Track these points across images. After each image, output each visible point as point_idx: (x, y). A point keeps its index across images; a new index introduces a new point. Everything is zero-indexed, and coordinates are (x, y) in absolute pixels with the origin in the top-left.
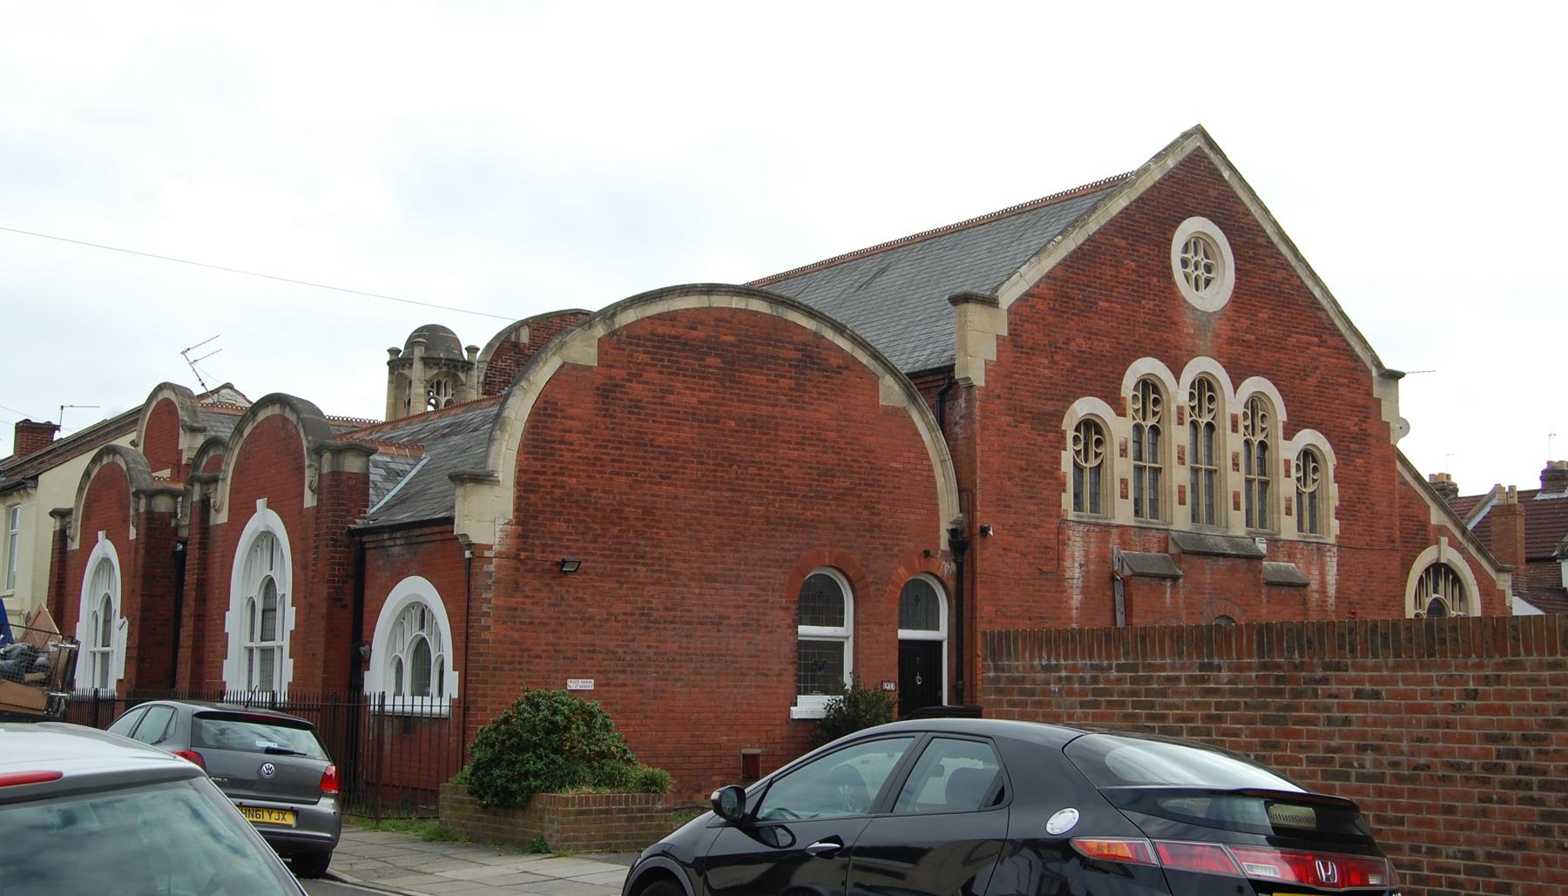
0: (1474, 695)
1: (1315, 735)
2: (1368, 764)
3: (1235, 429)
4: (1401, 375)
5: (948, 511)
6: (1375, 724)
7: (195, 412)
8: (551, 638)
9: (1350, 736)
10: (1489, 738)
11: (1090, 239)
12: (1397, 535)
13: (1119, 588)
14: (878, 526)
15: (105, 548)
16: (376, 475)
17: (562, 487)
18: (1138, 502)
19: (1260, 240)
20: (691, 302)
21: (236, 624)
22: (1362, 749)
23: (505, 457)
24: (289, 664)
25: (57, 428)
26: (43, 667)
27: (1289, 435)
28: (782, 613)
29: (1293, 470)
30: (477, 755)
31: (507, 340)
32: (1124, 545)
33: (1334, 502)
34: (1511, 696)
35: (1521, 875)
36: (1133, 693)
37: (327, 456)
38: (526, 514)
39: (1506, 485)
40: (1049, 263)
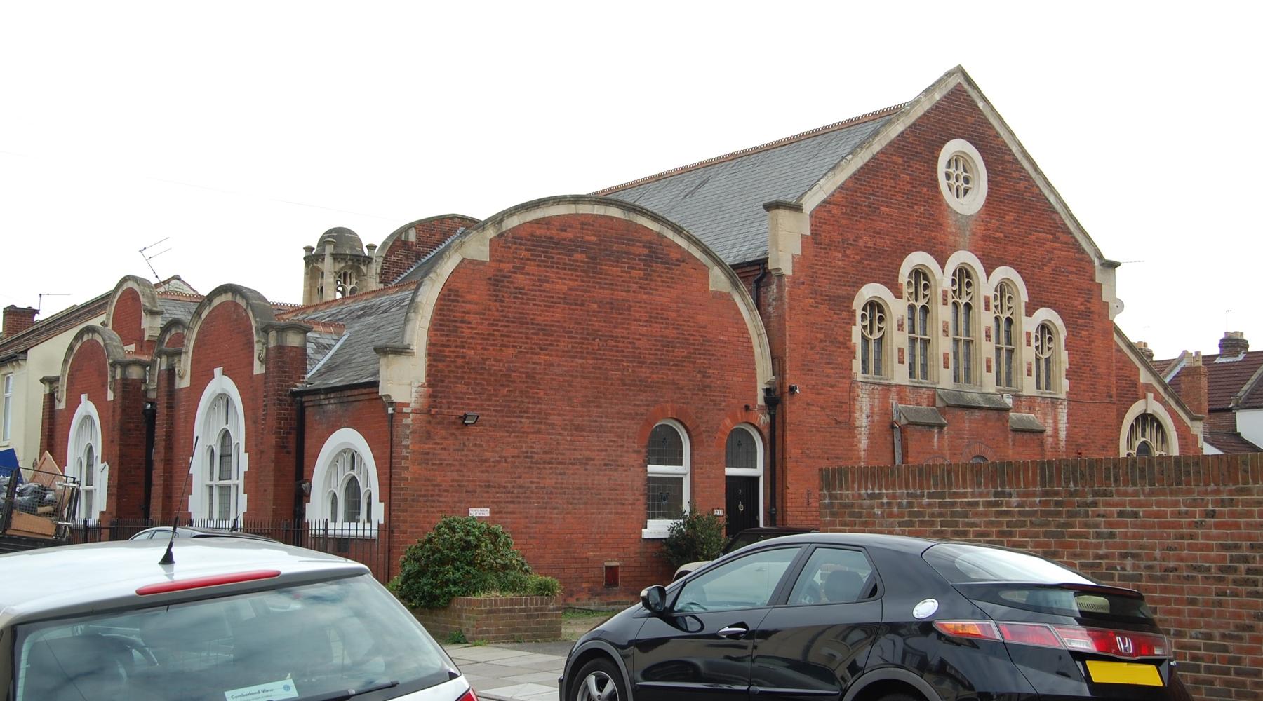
0: (1212, 514)
1: (1086, 546)
2: (1128, 568)
3: (987, 308)
4: (1118, 265)
5: (764, 374)
6: (1135, 536)
7: (153, 298)
8: (456, 476)
9: (1114, 546)
10: (1224, 547)
11: (874, 158)
12: (1114, 392)
13: (897, 435)
15: (87, 407)
16: (310, 348)
17: (463, 357)
18: (912, 366)
19: (1007, 157)
20: (562, 210)
21: (199, 468)
22: (1124, 556)
23: (418, 334)
24: (243, 498)
25: (37, 312)
26: (51, 502)
27: (1030, 313)
28: (635, 455)
29: (1033, 340)
30: (407, 568)
31: (398, 239)
32: (901, 400)
33: (1065, 365)
34: (1241, 515)
35: (1250, 651)
36: (941, 515)
37: (273, 334)
39: (1192, 351)
40: (841, 177)
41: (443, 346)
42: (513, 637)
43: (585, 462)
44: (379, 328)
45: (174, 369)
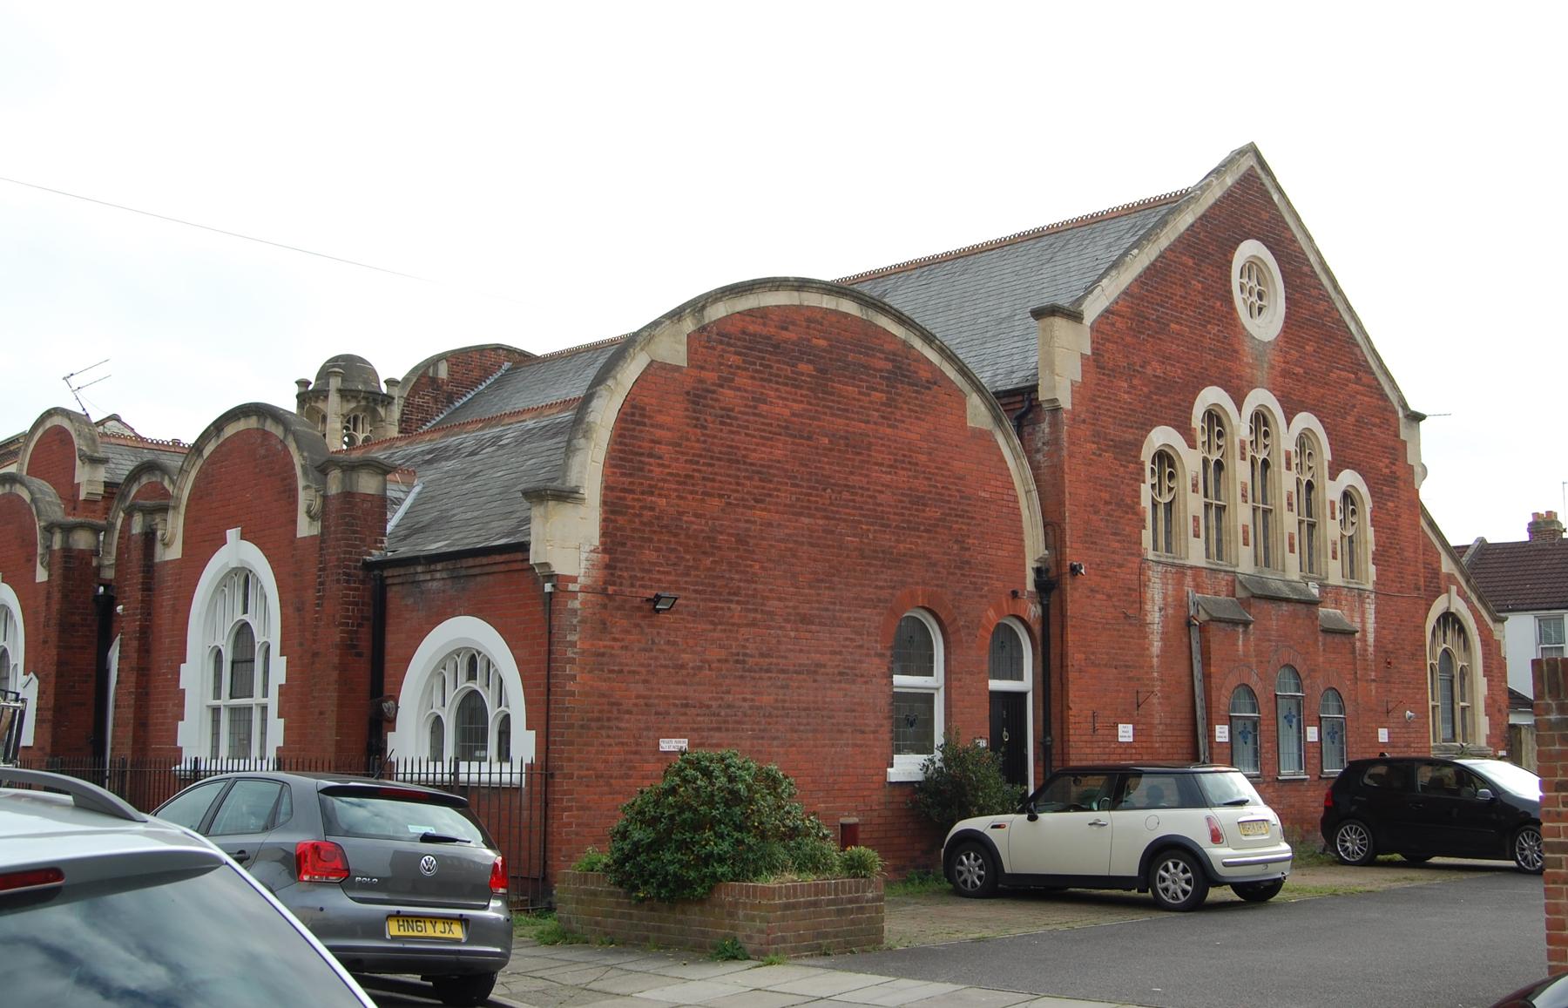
5: (1034, 548)
7: (94, 441)
8: (641, 688)
11: (1161, 256)
13: (1195, 635)
14: (968, 562)
17: (652, 509)
19: (1305, 269)
23: (589, 469)
27: (1333, 477)
28: (877, 661)
33: (1372, 547)
38: (614, 540)
41: (623, 490)
42: (819, 946)
43: (814, 670)
44: (475, 475)
45: (154, 533)
